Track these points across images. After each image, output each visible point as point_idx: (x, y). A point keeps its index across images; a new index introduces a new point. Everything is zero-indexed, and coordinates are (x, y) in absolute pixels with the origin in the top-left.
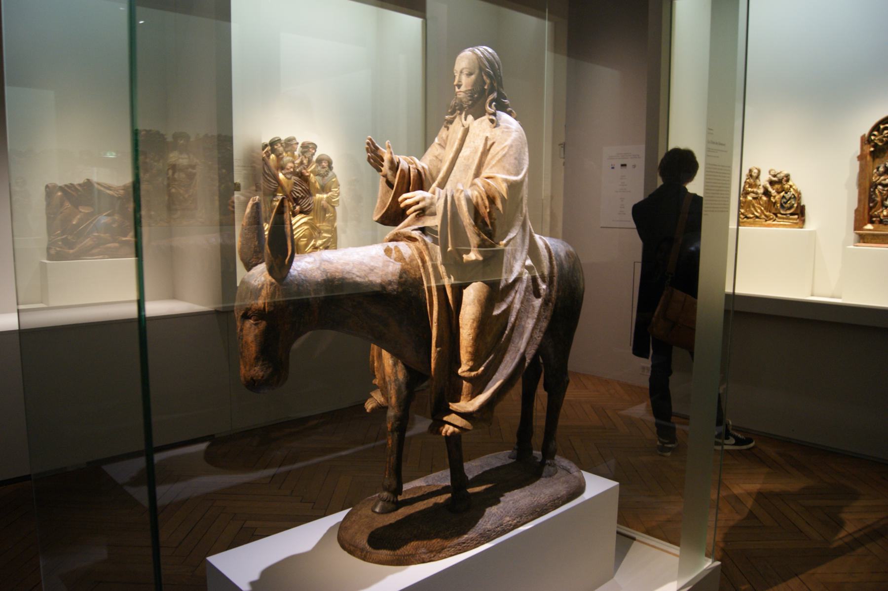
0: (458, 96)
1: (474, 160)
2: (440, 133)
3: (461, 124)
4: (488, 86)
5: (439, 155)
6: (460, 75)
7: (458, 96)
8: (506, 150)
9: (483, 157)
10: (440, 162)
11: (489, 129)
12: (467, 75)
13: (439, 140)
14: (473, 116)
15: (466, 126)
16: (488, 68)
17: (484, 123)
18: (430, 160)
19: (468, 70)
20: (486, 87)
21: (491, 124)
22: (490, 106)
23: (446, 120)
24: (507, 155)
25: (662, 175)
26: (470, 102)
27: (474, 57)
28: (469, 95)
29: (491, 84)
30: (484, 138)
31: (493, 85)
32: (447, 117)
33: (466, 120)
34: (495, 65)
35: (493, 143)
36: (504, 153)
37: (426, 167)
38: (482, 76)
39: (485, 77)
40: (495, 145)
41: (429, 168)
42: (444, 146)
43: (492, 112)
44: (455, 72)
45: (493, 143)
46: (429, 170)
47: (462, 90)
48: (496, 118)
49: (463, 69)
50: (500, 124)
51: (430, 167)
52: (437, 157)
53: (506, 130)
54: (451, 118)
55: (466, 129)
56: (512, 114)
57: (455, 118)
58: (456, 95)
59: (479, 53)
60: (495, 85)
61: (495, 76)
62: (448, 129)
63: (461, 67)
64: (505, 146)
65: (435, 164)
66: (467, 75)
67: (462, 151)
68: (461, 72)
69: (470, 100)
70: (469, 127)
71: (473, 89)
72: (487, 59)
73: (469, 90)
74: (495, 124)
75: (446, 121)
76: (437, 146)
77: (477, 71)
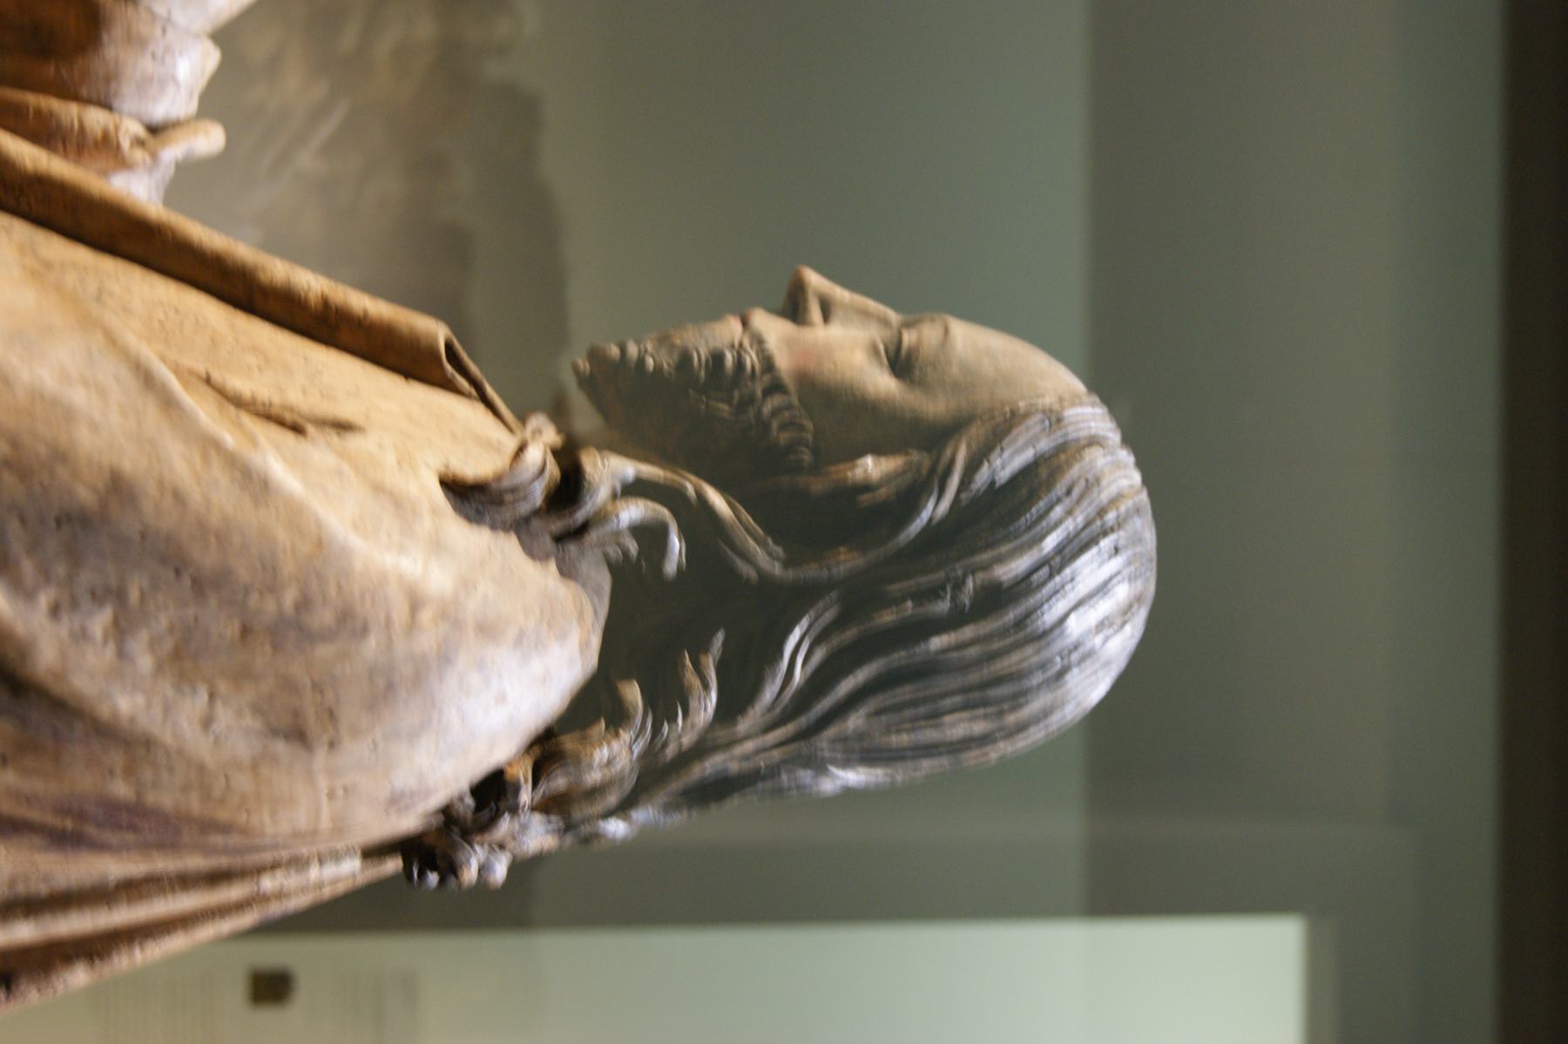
73: (768, 364)
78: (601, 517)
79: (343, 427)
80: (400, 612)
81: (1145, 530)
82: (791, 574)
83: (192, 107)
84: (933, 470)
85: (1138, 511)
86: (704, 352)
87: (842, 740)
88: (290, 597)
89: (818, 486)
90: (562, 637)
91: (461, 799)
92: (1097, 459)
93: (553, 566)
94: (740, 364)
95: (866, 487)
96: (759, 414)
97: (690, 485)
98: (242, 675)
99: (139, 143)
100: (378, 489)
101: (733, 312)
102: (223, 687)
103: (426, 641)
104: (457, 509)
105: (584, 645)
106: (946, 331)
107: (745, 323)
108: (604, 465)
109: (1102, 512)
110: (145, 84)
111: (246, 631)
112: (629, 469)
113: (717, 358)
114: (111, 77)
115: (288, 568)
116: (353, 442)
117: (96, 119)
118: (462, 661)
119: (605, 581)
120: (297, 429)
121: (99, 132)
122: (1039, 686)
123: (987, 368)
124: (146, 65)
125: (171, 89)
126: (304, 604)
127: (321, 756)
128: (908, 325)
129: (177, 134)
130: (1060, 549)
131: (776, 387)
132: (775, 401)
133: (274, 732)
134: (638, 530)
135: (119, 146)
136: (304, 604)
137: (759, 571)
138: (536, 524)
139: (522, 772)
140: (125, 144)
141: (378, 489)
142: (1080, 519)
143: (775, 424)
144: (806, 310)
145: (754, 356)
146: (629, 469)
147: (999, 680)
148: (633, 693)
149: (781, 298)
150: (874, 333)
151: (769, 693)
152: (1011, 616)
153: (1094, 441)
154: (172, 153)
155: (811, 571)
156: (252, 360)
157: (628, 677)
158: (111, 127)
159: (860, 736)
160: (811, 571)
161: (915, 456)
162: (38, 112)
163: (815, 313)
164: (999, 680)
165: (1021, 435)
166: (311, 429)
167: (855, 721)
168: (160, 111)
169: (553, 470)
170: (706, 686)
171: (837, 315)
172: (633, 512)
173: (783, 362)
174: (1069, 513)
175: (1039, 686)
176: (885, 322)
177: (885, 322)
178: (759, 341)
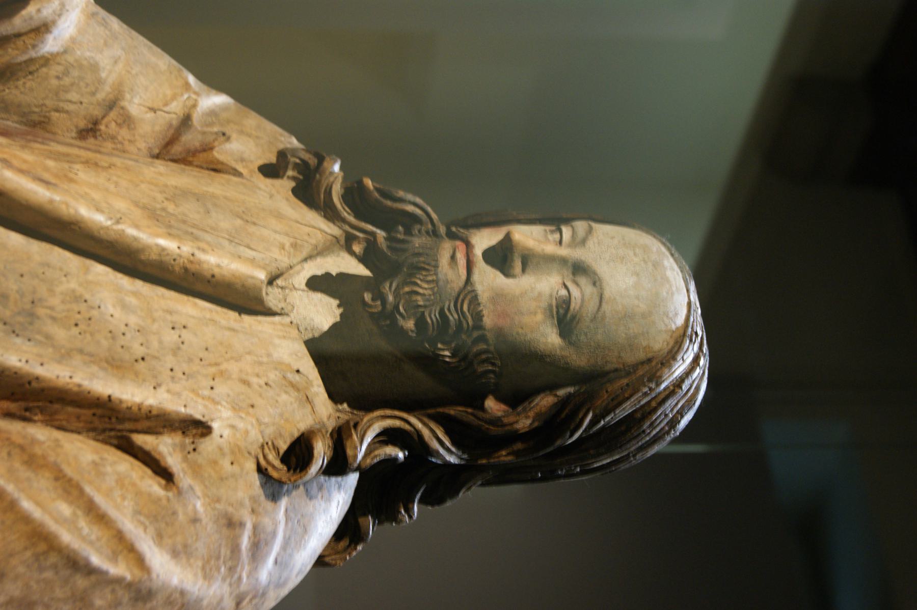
0: (446, 248)
1: (64, 355)
2: (253, 120)
3: (284, 261)
4: (496, 422)
5: (127, 121)
6: (563, 261)
7: (446, 248)
8: (119, 569)
9: (86, 413)
10: (82, 124)
11: (255, 436)
12: (566, 303)
13: (213, 113)
14: (334, 327)
15: (272, 298)
16: (593, 422)
17: (287, 399)
18: (94, 67)
19: (591, 306)
20: (491, 404)
21: (283, 447)
22: (388, 436)
23: (321, 159)
24: (81, 582)
25: (341, 403)
26: (410, 324)
27: (660, 343)
28: (453, 317)
29: (511, 438)
30: (197, 411)
31: (501, 448)
32: (336, 168)
33: (316, 284)
34: (610, 451)
35: (165, 474)
36: (96, 560)
37: (51, 44)
38: (551, 388)
39: (545, 401)
40: (153, 486)
41: (46, 61)
42: (177, 149)
43: (349, 452)
44: (581, 226)
45: (165, 474)
46: (31, 60)
47: (476, 277)
48: (368, 311)
49: (596, 281)
50: (284, 502)
51: (55, 70)
52: (112, 104)
53: (245, 542)
54: (329, 193)
55: (261, 301)
56: (343, 544)
57: (330, 213)
58: (452, 236)
59: (679, 369)
60: (504, 456)
61: (551, 456)
62: (270, 171)
63: (603, 269)
64: (140, 561)
65: (73, 96)
66: (566, 303)
67: (125, 281)
68: (579, 269)
69: (421, 323)
70: (269, 313)
71: (483, 339)
72: (647, 412)
73: (478, 317)
74: (278, 470)
75: (312, 161)
76: (177, 107)
77: (579, 360)
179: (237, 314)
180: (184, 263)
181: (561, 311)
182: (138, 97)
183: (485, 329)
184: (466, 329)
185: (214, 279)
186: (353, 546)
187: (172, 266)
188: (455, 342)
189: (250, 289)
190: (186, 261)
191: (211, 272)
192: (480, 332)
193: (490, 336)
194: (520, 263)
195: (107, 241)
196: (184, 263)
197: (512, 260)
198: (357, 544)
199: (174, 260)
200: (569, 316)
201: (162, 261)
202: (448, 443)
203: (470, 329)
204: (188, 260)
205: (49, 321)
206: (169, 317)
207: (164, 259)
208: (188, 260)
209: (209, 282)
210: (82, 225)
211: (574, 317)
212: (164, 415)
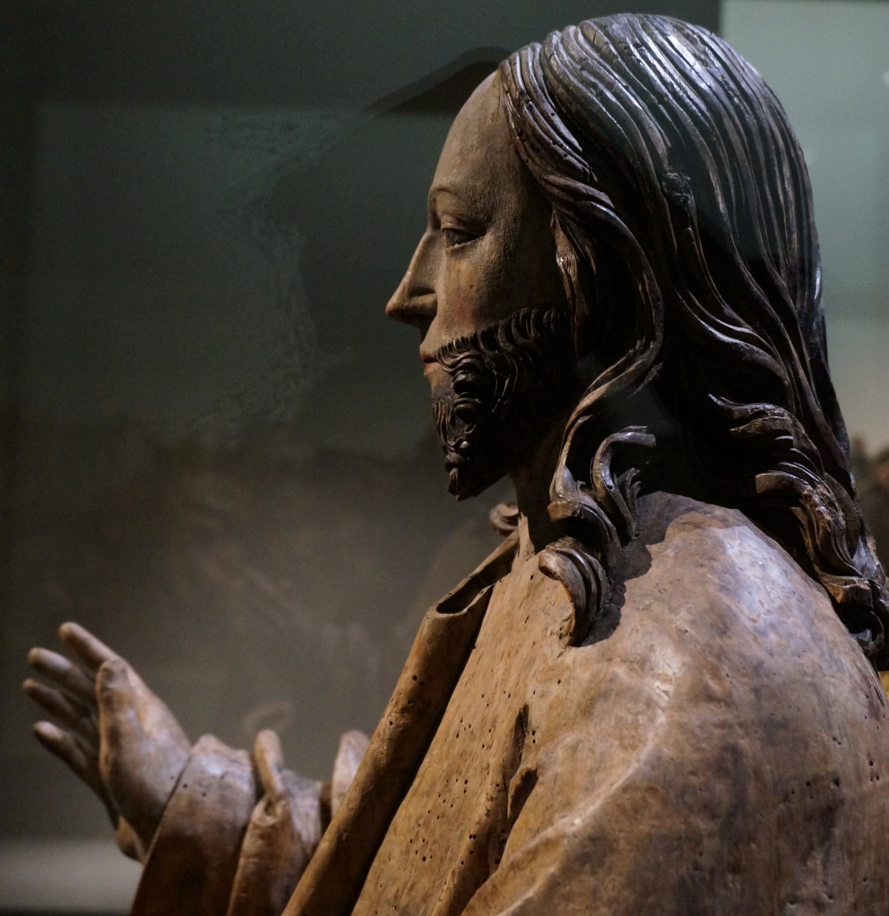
73: (463, 344)
78: (608, 502)
79: (522, 721)
80: (708, 713)
81: (619, 24)
82: (659, 334)
83: (242, 755)
84: (570, 206)
85: (603, 28)
86: (457, 398)
87: (793, 290)
88: (703, 824)
89: (582, 307)
90: (719, 544)
91: (862, 643)
92: (560, 60)
93: (653, 548)
94: (466, 368)
95: (583, 263)
96: (510, 354)
97: (576, 419)
98: (777, 872)
99: (269, 808)
100: (586, 711)
101: (423, 369)
102: (786, 890)
103: (741, 691)
104: (606, 635)
105: (725, 523)
106: (442, 189)
107: (430, 360)
108: (744, 684)
109: (607, 57)
110: (223, 801)
111: (735, 869)
112: (562, 475)
113: (459, 387)
114: (219, 827)
115: (675, 824)
116: (535, 717)
117: (250, 844)
118: (756, 652)
119: (659, 497)
120: (530, 779)
121: (260, 842)
122: (757, 117)
123: (476, 155)
124: (211, 799)
125: (229, 779)
126: (709, 810)
127: (846, 791)
128: (437, 224)
129: (264, 778)
130: (641, 94)
131: (489, 337)
132: (500, 337)
133: (827, 837)
134: (616, 469)
135: (273, 827)
136: (709, 810)
137: (656, 362)
138: (613, 562)
139: (841, 587)
140: (270, 820)
141: (586, 711)
142: (614, 77)
143: (521, 341)
144: (423, 307)
145: (461, 356)
146: (562, 475)
147: (752, 152)
148: (764, 479)
149: (413, 330)
150: (442, 253)
151: (763, 356)
152: (699, 139)
153: (544, 62)
154: (277, 781)
155: (657, 317)
156: (457, 786)
157: (753, 483)
158: (258, 831)
159: (791, 274)
160: (657, 317)
161: (554, 219)
162: (244, 890)
163: (427, 300)
164: (752, 152)
165: (540, 126)
166: (527, 764)
167: (782, 281)
168: (245, 787)
169: (565, 544)
170: (762, 413)
171: (424, 281)
172: (602, 472)
173: (467, 331)
174: (610, 86)
175: (757, 117)
176: (431, 242)
177: (431, 242)
178: (446, 350)
179: (474, 651)
180: (396, 712)
181: (457, 238)
182: (660, 712)
183: (476, 335)
184: (474, 360)
185: (418, 677)
186: (802, 502)
187: (398, 726)
188: (494, 371)
189: (433, 634)
190: (395, 710)
191: (411, 679)
192: (479, 339)
193: (483, 328)
194: (420, 298)
195: (362, 800)
196: (396, 712)
197: (414, 308)
198: (799, 495)
199: (391, 723)
200: (462, 228)
201: (390, 739)
202: (814, 389)
203: (477, 353)
204: (394, 707)
205: (413, 894)
206: (449, 739)
207: (387, 736)
208: (394, 707)
209: (421, 684)
210: (342, 828)
211: (459, 221)
212: (504, 767)
